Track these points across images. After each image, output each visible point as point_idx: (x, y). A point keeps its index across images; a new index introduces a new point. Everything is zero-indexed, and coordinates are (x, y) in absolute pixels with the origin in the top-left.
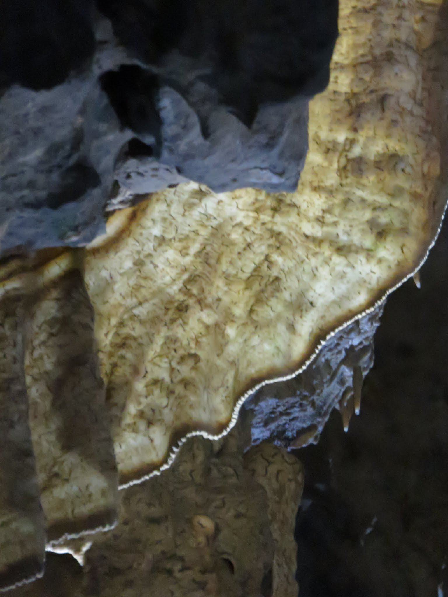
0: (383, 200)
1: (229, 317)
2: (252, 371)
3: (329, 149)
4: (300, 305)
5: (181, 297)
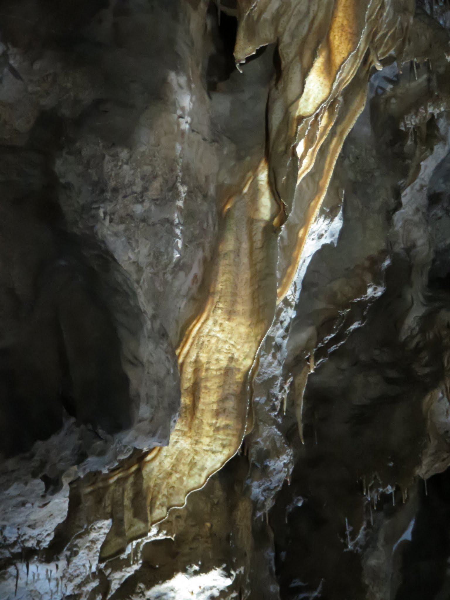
0: (224, 437)
1: (184, 475)
2: (188, 489)
3: (211, 425)
4: (203, 469)
5: (171, 471)
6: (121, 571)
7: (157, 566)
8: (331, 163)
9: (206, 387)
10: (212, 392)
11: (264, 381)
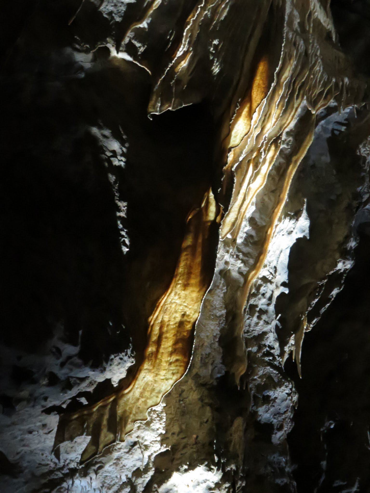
6: (141, 477)
7: (163, 470)
8: (288, 181)
9: (166, 338)
10: (170, 340)
11: (254, 336)
